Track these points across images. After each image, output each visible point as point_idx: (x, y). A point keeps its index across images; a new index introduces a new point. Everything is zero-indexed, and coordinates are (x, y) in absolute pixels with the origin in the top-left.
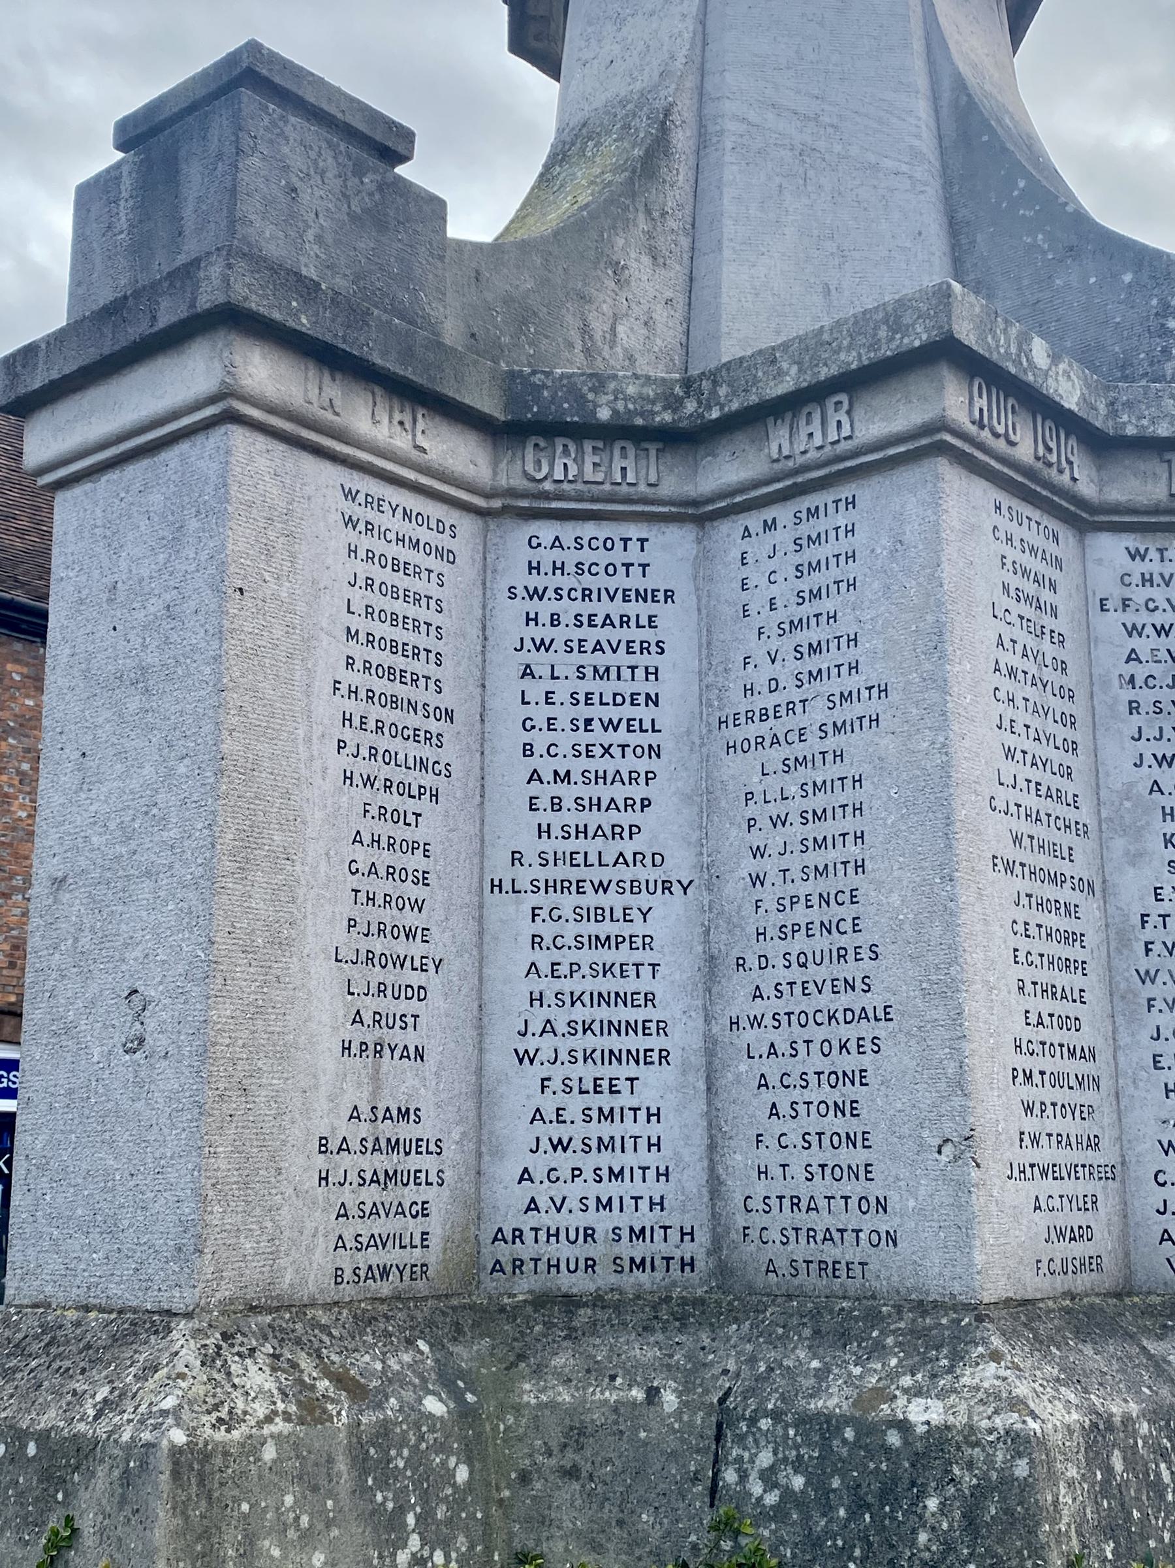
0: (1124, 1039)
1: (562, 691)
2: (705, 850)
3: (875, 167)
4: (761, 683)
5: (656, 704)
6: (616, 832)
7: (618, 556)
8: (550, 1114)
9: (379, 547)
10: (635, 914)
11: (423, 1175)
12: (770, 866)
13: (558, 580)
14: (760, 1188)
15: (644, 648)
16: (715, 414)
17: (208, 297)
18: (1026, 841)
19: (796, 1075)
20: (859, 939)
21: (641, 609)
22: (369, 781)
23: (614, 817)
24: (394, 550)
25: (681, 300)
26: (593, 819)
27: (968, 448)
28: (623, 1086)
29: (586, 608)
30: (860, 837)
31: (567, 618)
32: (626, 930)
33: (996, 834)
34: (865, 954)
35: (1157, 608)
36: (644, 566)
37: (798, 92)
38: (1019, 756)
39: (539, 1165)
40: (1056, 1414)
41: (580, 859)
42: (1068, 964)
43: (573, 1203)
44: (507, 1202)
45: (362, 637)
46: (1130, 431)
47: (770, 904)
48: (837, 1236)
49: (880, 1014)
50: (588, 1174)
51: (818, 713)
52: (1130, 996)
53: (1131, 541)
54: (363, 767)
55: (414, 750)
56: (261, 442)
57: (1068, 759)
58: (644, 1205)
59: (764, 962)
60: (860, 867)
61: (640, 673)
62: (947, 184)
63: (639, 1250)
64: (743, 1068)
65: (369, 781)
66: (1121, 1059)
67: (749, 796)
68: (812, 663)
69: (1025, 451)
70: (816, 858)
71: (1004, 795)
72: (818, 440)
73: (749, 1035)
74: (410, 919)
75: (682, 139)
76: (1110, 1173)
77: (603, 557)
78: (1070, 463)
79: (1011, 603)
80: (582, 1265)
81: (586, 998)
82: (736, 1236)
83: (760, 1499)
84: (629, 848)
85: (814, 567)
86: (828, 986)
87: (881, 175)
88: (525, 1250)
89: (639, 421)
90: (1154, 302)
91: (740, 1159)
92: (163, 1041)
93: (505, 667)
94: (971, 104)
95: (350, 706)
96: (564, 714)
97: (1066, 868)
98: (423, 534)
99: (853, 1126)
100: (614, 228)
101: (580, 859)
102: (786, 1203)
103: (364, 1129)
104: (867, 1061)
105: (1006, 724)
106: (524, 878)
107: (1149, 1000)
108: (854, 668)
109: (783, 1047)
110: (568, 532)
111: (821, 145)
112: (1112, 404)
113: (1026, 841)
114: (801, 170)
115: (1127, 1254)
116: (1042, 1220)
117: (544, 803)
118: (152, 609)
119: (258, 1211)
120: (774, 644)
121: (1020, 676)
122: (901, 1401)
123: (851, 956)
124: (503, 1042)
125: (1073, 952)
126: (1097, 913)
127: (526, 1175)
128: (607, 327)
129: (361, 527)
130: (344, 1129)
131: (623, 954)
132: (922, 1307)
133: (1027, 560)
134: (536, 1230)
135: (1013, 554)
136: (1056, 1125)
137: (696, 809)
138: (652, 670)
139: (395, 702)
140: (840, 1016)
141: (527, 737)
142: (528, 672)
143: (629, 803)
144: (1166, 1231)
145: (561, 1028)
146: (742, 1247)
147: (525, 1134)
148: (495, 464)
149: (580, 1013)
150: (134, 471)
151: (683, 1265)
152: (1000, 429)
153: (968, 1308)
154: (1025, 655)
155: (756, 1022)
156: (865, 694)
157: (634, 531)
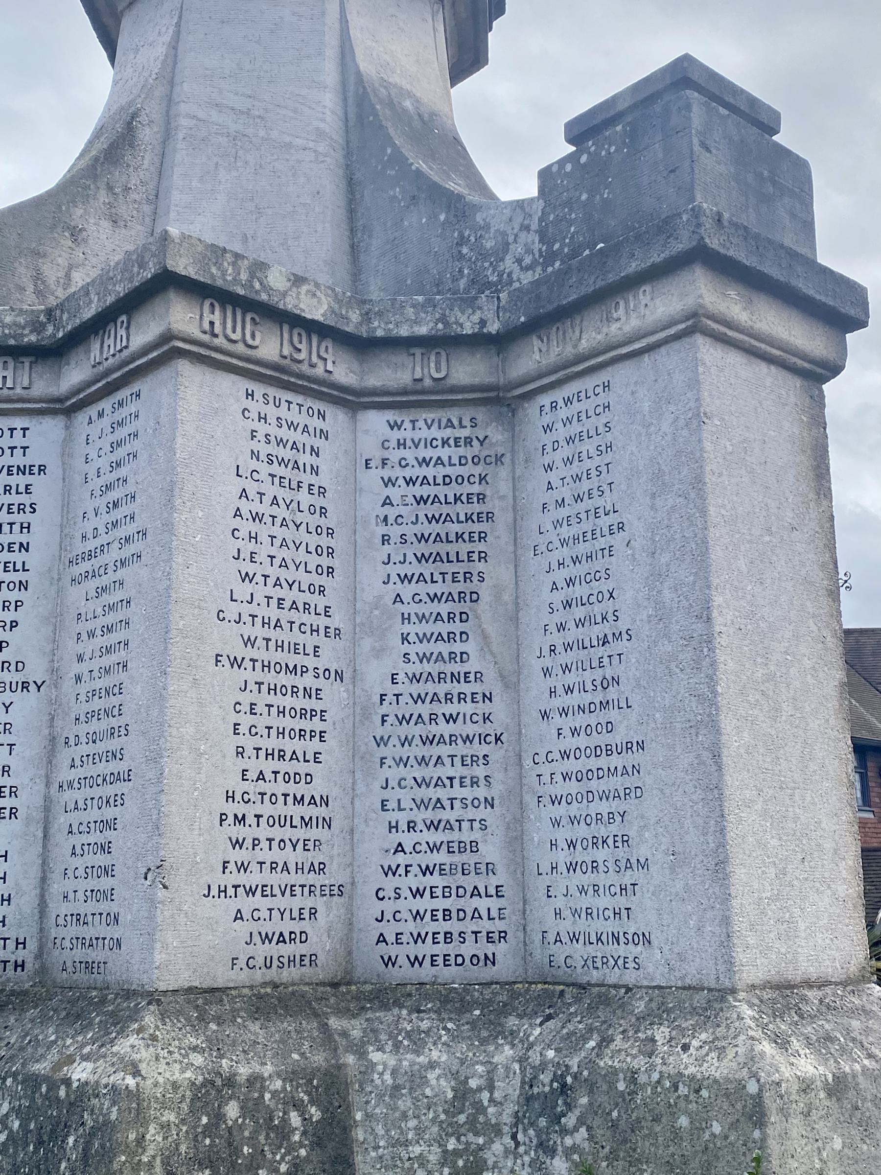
0: (361, 788)
2: (56, 658)
3: (289, 145)
5: (27, 551)
15: (21, 508)
21: (21, 480)
27: (202, 351)
35: (407, 465)
37: (237, 94)
46: (380, 333)
52: (368, 756)
53: (391, 415)
62: (348, 154)
66: (357, 803)
75: (147, 135)
87: (293, 151)
89: (12, 342)
90: (456, 234)
91: (57, 887)
100: (73, 202)
107: (382, 759)
111: (250, 131)
112: (367, 314)
114: (234, 151)
115: (350, 953)
116: (243, 929)
126: (345, 695)
128: (61, 274)
137: (51, 628)
138: (25, 525)
144: (382, 934)
157: (18, 422)
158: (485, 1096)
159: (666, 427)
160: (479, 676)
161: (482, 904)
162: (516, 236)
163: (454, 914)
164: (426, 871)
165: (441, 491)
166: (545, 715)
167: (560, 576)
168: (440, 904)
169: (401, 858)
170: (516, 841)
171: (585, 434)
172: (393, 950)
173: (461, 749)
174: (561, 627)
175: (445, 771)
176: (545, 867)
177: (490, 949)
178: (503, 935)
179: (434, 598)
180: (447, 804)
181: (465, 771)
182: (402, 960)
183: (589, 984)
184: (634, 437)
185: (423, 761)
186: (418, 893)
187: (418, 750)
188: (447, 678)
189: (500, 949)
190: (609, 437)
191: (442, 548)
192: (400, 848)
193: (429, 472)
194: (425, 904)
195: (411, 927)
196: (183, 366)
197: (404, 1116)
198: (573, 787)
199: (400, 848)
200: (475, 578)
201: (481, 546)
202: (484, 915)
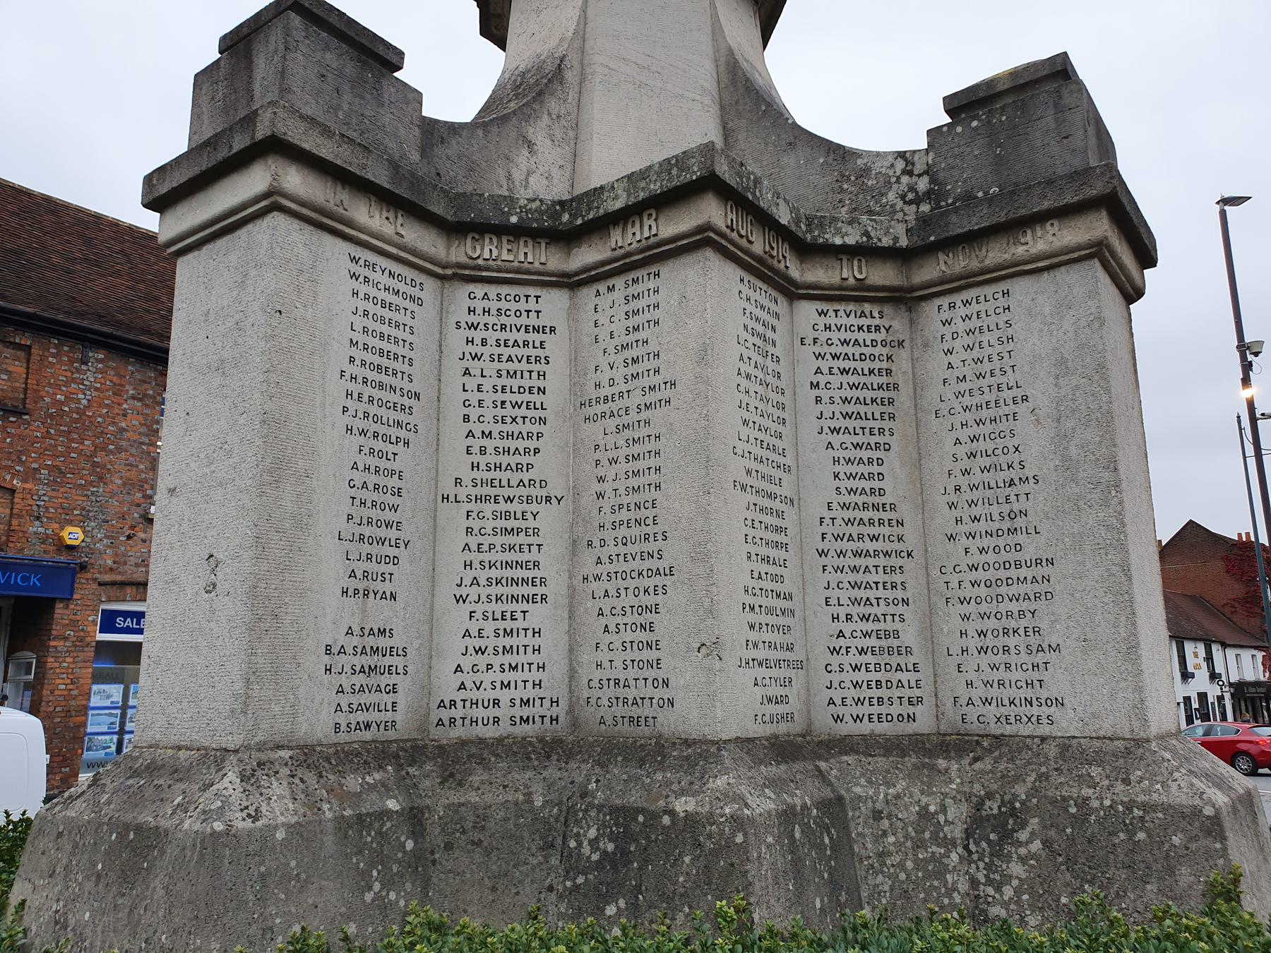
1: (487, 384)
3: (682, 96)
4: (605, 382)
6: (519, 467)
7: (522, 305)
8: (474, 633)
9: (373, 292)
10: (529, 516)
11: (394, 669)
12: (607, 487)
13: (486, 319)
14: (597, 675)
16: (579, 221)
17: (261, 132)
18: (754, 473)
19: (619, 608)
20: (656, 529)
21: (538, 338)
22: (363, 432)
23: (517, 459)
24: (382, 295)
25: (569, 166)
26: (505, 460)
28: (519, 615)
29: (503, 336)
30: (658, 470)
31: (492, 341)
32: (523, 525)
33: (737, 467)
34: (660, 537)
36: (538, 312)
38: (751, 424)
39: (466, 663)
40: (762, 804)
41: (496, 483)
42: (777, 545)
43: (487, 684)
44: (447, 686)
45: (360, 346)
47: (607, 509)
48: (640, 701)
49: (667, 572)
50: (497, 668)
51: (637, 399)
54: (360, 424)
55: (393, 415)
56: (296, 224)
57: (780, 428)
58: (529, 685)
59: (603, 543)
60: (658, 487)
61: (535, 375)
62: (722, 108)
63: (526, 712)
64: (589, 604)
65: (363, 432)
67: (597, 447)
68: (633, 369)
69: (758, 248)
70: (634, 482)
71: (741, 447)
72: (638, 237)
73: (594, 585)
74: (389, 515)
76: (799, 665)
77: (513, 306)
78: (784, 257)
79: (749, 337)
80: (491, 721)
81: (498, 565)
82: (583, 703)
83: (589, 857)
84: (526, 477)
85: (636, 313)
86: (638, 557)
88: (457, 713)
91: (587, 657)
92: (227, 585)
93: (453, 368)
94: (736, 62)
95: (352, 386)
96: (488, 398)
97: (777, 490)
98: (402, 287)
99: (650, 637)
101: (496, 483)
102: (612, 683)
103: (355, 641)
104: (659, 599)
105: (744, 405)
106: (462, 493)
108: (657, 371)
109: (612, 592)
110: (493, 290)
111: (650, 82)
113: (754, 473)
115: (809, 712)
117: (475, 450)
118: (229, 325)
119: (284, 689)
120: (612, 358)
121: (753, 379)
122: (672, 799)
123: (651, 539)
124: (447, 590)
125: (780, 538)
127: (459, 669)
128: (523, 177)
129: (361, 279)
130: (342, 640)
131: (522, 539)
132: (687, 743)
133: (758, 312)
134: (464, 701)
135: (750, 308)
136: (769, 637)
139: (381, 386)
140: (645, 573)
141: (466, 411)
142: (467, 372)
143: (527, 451)
145: (483, 581)
146: (586, 708)
147: (460, 644)
148: (448, 248)
149: (494, 573)
150: (222, 243)
151: (552, 720)
152: (743, 233)
153: (713, 743)
154: (756, 367)
155: (598, 578)
156: (663, 386)
157: (532, 291)
158: (942, 818)
159: (1067, 325)
160: (893, 507)
161: (904, 677)
162: (898, 178)
163: (884, 685)
164: (862, 651)
165: (859, 365)
166: (951, 538)
167: (964, 434)
168: (874, 676)
169: (842, 641)
170: (929, 630)
171: (985, 328)
172: (841, 710)
173: (882, 561)
174: (966, 472)
175: (872, 578)
176: (955, 650)
177: (911, 710)
178: (920, 700)
179: (856, 446)
180: (874, 602)
181: (887, 578)
182: (848, 718)
183: (1003, 735)
184: (1035, 333)
185: (855, 569)
186: (856, 668)
187: (851, 561)
188: (869, 509)
189: (918, 710)
190: (1010, 331)
191: (862, 409)
192: (841, 634)
193: (850, 350)
194: (861, 676)
195: (853, 693)
196: (709, 253)
197: (885, 834)
198: (983, 591)
199: (841, 634)
200: (887, 433)
201: (890, 409)
202: (906, 685)
